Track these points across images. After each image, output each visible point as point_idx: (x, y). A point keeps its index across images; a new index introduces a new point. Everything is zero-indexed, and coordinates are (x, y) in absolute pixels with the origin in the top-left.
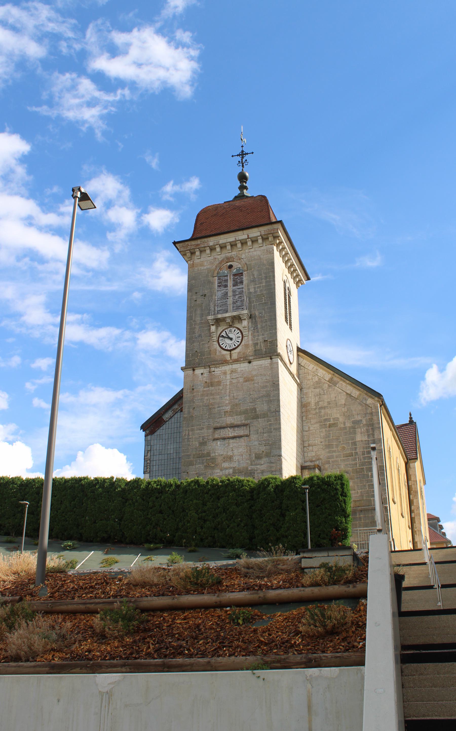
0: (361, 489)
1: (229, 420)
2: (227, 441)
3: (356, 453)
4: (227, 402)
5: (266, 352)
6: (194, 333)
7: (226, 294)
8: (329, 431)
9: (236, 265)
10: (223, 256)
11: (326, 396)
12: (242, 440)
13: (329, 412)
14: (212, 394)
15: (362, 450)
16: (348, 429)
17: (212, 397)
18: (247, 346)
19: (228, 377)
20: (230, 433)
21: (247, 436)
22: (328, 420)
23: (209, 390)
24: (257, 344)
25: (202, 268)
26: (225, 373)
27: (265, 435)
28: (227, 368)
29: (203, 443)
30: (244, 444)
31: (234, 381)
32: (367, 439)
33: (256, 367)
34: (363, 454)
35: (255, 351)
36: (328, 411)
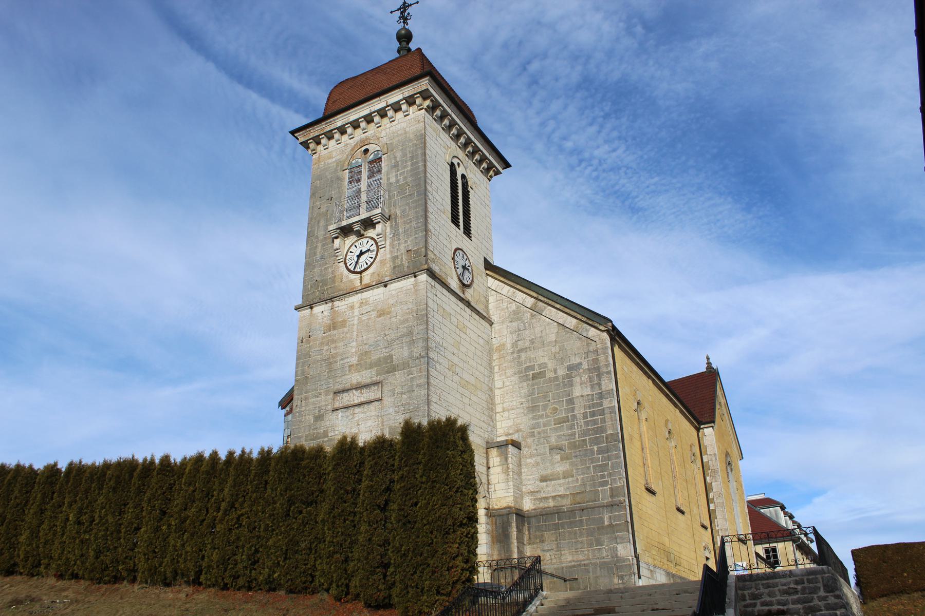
0: (583, 474)
1: (356, 378)
2: (351, 411)
3: (574, 417)
4: (354, 350)
5: (408, 267)
6: (315, 254)
7: (359, 191)
8: (533, 385)
9: (372, 148)
10: (357, 139)
11: (527, 332)
12: (372, 407)
13: (533, 356)
14: (334, 341)
15: (582, 411)
16: (561, 380)
17: (333, 346)
18: (383, 262)
19: (356, 312)
20: (356, 397)
21: (378, 400)
22: (531, 368)
23: (330, 336)
24: (397, 256)
25: (330, 161)
26: (352, 307)
27: (404, 396)
28: (355, 299)
29: (319, 418)
30: (374, 413)
31: (364, 318)
32: (589, 393)
33: (394, 292)
34: (585, 417)
35: (395, 267)
36: (531, 354)
